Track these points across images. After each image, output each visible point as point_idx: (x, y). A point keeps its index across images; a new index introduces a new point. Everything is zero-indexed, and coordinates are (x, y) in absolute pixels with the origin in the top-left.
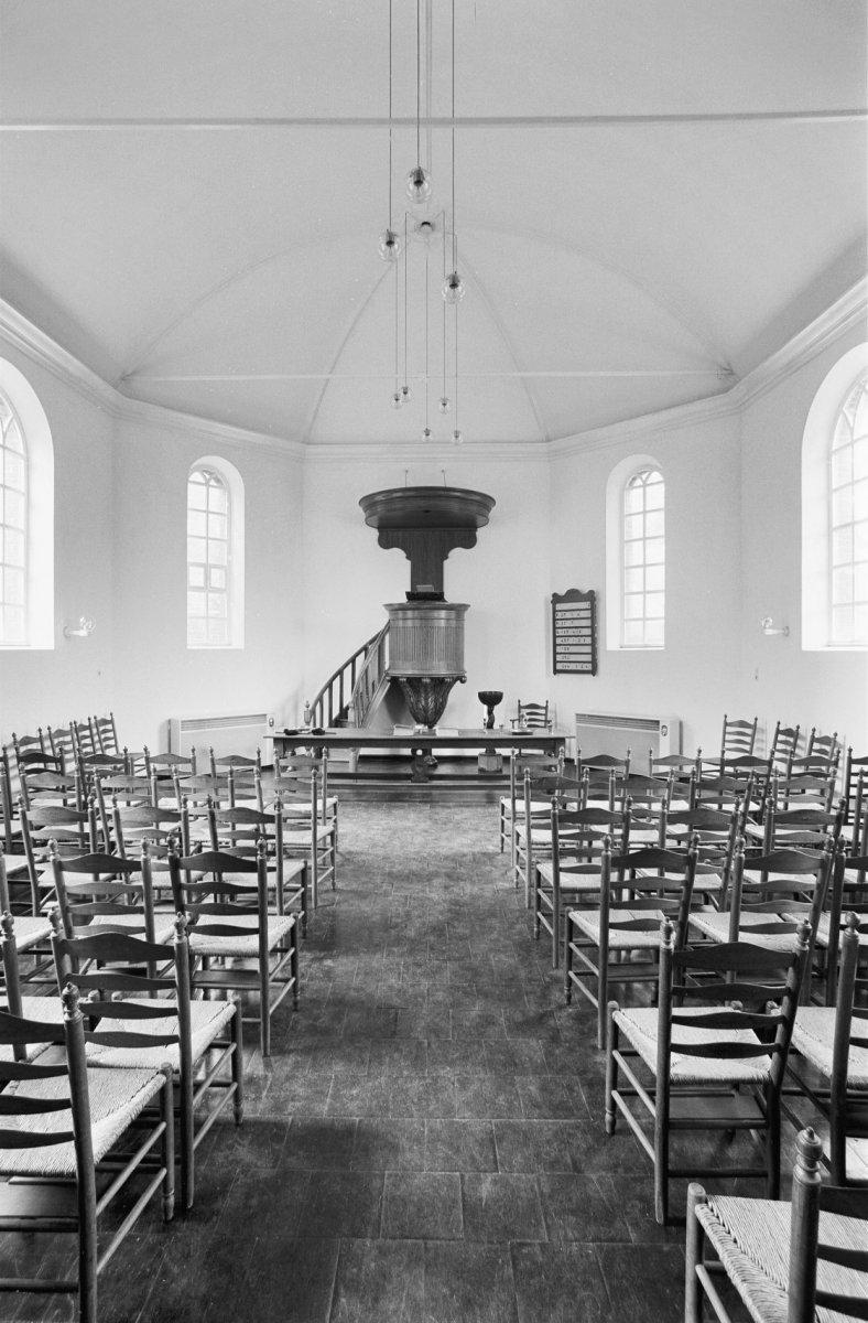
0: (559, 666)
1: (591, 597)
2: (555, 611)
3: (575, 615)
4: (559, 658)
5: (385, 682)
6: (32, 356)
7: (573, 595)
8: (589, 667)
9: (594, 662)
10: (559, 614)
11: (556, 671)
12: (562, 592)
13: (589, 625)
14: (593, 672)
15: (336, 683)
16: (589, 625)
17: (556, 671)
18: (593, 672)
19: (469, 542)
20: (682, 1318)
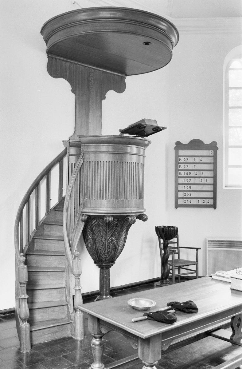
0: (180, 202)
1: (213, 147)
2: (177, 156)
3: (197, 160)
4: (181, 195)
5: (81, 222)
6: (53, 252)
7: (196, 144)
8: (211, 202)
9: (215, 198)
10: (182, 165)
11: (177, 206)
12: (185, 141)
13: (212, 182)
14: (214, 206)
15: (55, 172)
16: (212, 169)
17: (177, 206)
18: (214, 206)
19: (120, 88)
20: (241, 251)
